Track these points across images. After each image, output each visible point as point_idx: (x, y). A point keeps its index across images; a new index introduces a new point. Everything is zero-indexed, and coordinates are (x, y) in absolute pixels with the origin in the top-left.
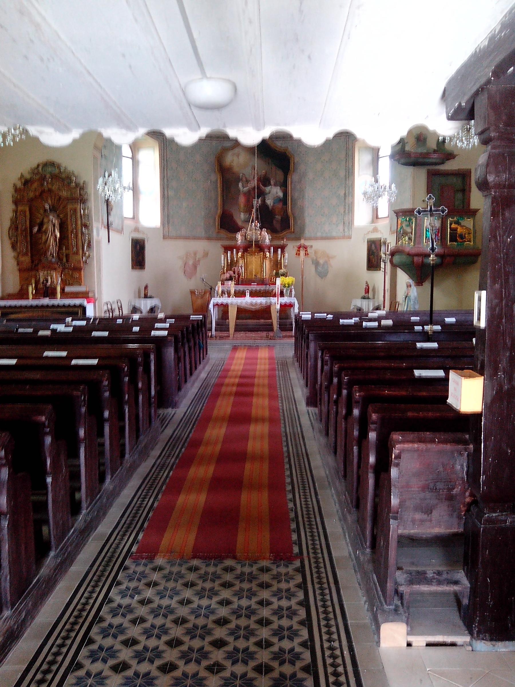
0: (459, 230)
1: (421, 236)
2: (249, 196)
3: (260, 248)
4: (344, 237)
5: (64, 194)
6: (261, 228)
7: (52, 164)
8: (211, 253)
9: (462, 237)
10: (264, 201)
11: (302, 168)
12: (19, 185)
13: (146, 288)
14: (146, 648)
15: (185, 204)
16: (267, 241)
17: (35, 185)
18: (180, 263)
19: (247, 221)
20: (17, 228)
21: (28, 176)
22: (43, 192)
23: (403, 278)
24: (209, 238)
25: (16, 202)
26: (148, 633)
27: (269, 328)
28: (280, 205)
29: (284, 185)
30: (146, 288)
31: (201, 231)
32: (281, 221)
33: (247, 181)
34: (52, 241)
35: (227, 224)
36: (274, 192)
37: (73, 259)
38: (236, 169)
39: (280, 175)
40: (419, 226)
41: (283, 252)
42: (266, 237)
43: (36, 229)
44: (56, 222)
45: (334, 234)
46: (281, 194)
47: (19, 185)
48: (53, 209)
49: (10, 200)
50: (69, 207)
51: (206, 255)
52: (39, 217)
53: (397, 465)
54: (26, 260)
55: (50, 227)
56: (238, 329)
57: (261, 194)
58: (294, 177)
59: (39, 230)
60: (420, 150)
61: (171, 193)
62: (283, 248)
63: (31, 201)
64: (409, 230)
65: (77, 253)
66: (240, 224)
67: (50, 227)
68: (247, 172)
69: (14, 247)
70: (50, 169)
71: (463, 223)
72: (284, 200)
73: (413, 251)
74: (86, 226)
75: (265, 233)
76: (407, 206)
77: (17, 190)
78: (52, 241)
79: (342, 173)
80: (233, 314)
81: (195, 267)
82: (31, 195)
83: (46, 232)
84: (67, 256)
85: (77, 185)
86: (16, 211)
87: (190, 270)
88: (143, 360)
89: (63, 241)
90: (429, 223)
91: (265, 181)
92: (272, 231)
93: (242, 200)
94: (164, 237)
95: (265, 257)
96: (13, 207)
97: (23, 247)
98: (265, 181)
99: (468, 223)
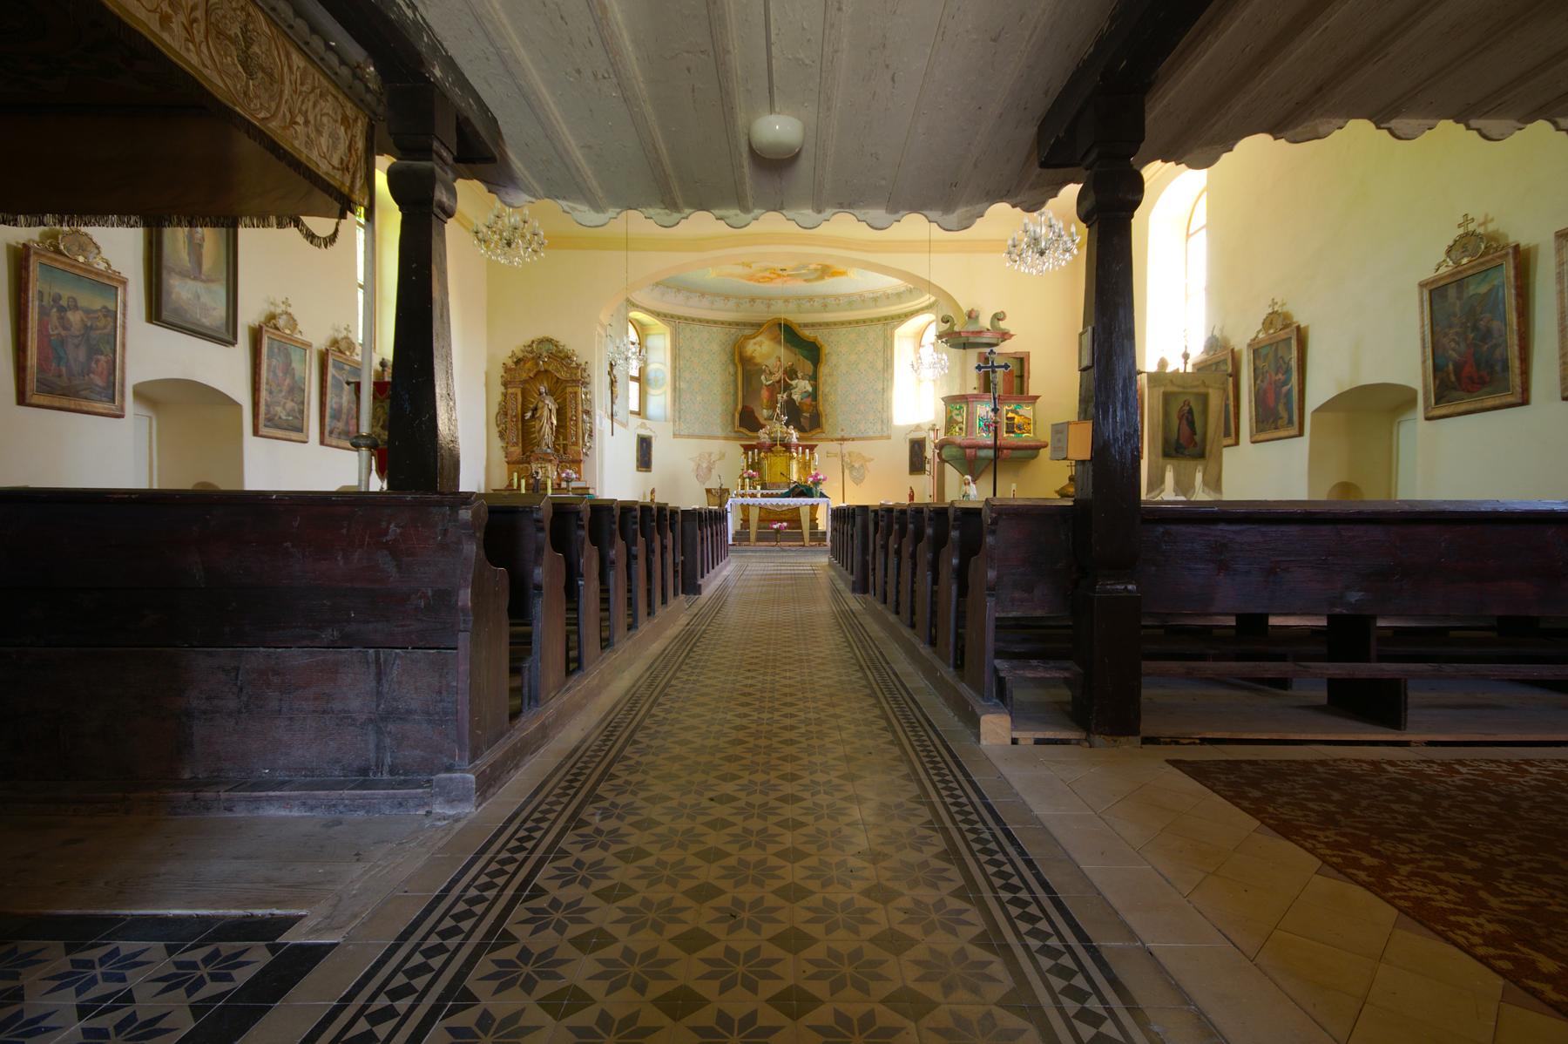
0: (1017, 420)
1: (973, 426)
2: (773, 390)
3: (787, 447)
4: (881, 438)
5: (563, 375)
6: (787, 424)
7: (550, 341)
8: (728, 458)
9: (1019, 428)
10: (790, 396)
11: (833, 359)
12: (510, 363)
13: (653, 492)
14: (628, 954)
15: (699, 398)
16: (794, 440)
17: (529, 365)
18: (693, 465)
19: (770, 418)
20: (506, 414)
21: (520, 355)
22: (538, 373)
23: (951, 473)
24: (726, 438)
25: (505, 385)
26: (613, 977)
27: (800, 537)
28: (808, 401)
29: (814, 378)
30: (653, 492)
31: (719, 432)
32: (807, 418)
33: (771, 373)
34: (547, 429)
35: (747, 421)
36: (802, 386)
37: (571, 449)
38: (758, 360)
39: (809, 366)
40: (971, 414)
41: (812, 453)
42: (794, 436)
43: (529, 414)
44: (554, 407)
45: (871, 434)
46: (810, 389)
47: (510, 363)
48: (550, 393)
49: (499, 381)
50: (569, 390)
51: (722, 456)
52: (533, 402)
53: (993, 532)
54: (516, 450)
55: (546, 413)
56: (758, 539)
57: (788, 387)
58: (824, 370)
59: (533, 416)
60: (971, 328)
61: (683, 385)
62: (812, 448)
63: (525, 382)
64: (959, 419)
65: (576, 444)
66: (762, 421)
67: (546, 413)
68: (771, 363)
69: (502, 435)
70: (547, 346)
71: (1021, 412)
72: (814, 395)
73: (966, 442)
74: (587, 413)
75: (792, 430)
76: (956, 392)
77: (507, 370)
78: (547, 429)
79: (880, 365)
80: (754, 515)
81: (710, 469)
82: (524, 376)
83: (540, 418)
84: (565, 446)
85: (578, 366)
86: (505, 395)
87: (703, 472)
88: (665, 543)
89: (561, 429)
90: (983, 410)
91: (791, 373)
92: (800, 428)
93: (765, 393)
94: (675, 436)
95: (792, 458)
96: (502, 389)
97: (513, 436)
98: (791, 373)
99: (1026, 410)
